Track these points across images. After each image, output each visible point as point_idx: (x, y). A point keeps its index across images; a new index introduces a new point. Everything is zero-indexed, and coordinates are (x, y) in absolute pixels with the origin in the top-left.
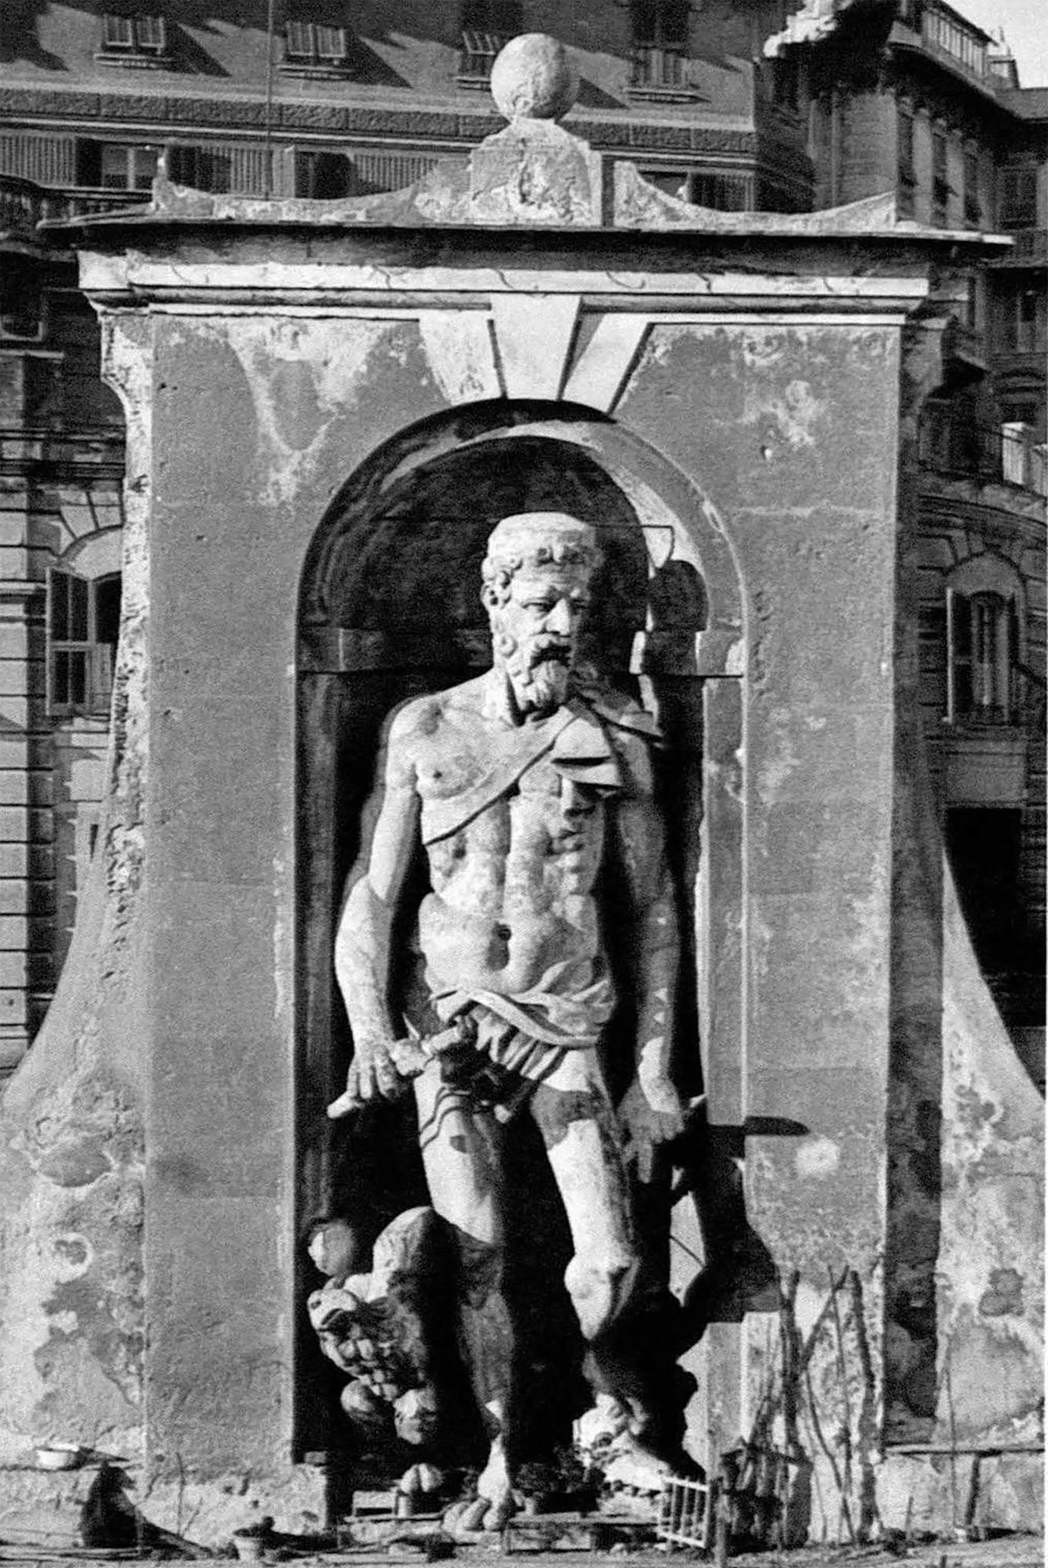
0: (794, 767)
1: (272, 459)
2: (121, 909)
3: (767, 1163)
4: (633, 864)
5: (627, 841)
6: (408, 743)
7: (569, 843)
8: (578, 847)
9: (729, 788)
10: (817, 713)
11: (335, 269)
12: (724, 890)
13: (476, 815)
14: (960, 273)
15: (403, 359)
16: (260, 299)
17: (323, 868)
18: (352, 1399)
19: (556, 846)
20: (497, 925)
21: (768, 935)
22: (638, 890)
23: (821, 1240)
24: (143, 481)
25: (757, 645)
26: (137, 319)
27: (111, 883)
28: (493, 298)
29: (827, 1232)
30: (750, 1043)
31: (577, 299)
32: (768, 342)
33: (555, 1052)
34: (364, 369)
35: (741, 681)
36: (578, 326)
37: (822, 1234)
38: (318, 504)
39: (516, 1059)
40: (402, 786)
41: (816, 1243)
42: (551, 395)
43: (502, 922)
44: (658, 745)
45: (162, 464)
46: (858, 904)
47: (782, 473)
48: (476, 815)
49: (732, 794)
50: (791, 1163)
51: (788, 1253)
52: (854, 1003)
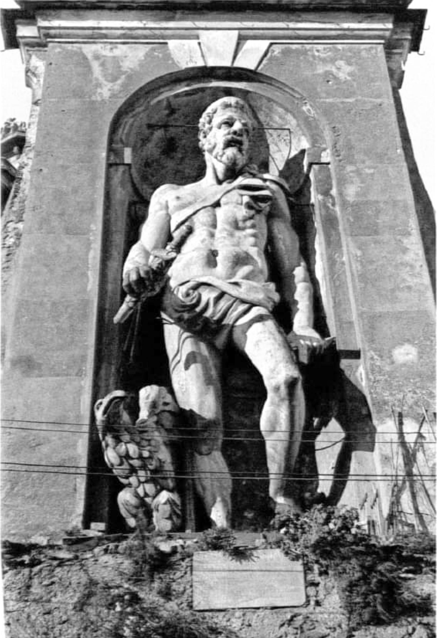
0: (361, 187)
1: (99, 85)
2: (8, 255)
3: (376, 357)
4: (283, 247)
5: (280, 236)
6: (165, 199)
7: (249, 223)
8: (253, 226)
9: (330, 205)
10: (370, 168)
11: (129, 22)
12: (333, 244)
13: (198, 210)
14: (405, 30)
15: (160, 55)
16: (95, 36)
17: (119, 239)
18: (125, 497)
19: (241, 224)
20: (211, 250)
21: (359, 253)
22: (287, 262)
23: (415, 396)
24: (39, 102)
25: (336, 144)
26: (42, 52)
27: (4, 244)
28: (200, 32)
29: (418, 391)
30: (356, 300)
31: (236, 33)
32: (325, 49)
33: (246, 306)
34: (143, 58)
35: (330, 166)
36: (238, 44)
37: (415, 393)
38: (120, 100)
39: (224, 308)
40: (161, 210)
41: (412, 398)
42: (227, 63)
43: (213, 249)
44: (291, 199)
45: (48, 87)
46: (405, 241)
47: (338, 88)
48: (198, 210)
49: (331, 207)
50: (391, 357)
51: (397, 403)
52: (411, 281)
